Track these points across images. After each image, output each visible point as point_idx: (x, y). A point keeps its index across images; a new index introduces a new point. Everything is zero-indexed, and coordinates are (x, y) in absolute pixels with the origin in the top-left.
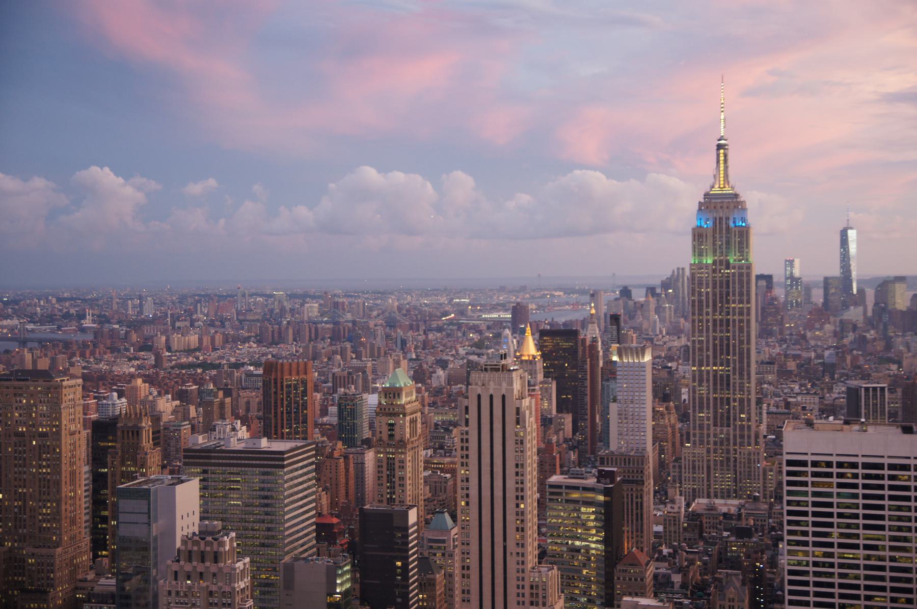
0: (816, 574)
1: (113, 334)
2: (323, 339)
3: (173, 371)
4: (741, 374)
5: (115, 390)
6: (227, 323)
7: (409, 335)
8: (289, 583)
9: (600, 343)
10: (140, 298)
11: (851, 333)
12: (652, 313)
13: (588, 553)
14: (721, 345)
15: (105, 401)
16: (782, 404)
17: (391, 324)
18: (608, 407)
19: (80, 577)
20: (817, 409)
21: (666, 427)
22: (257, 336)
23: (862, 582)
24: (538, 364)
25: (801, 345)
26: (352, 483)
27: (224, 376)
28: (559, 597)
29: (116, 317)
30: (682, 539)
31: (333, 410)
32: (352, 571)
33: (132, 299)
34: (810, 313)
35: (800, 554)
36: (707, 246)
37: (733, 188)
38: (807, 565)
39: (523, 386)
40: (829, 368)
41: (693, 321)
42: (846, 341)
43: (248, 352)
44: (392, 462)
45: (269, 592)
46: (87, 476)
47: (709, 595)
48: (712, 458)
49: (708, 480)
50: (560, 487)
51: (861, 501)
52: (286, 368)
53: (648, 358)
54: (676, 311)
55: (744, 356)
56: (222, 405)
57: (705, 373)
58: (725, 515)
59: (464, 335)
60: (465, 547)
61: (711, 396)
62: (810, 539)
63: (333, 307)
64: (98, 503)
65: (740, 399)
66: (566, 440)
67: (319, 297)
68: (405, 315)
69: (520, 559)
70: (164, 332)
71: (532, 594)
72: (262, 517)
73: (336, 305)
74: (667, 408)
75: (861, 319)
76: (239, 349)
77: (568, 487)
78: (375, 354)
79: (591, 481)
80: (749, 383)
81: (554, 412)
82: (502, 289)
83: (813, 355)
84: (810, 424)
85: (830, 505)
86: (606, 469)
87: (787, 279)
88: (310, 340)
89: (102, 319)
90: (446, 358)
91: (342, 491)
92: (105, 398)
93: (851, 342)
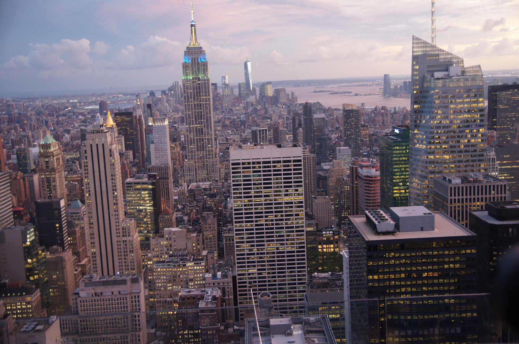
0: (245, 209)
4: (208, 128)
12: (165, 103)
14: (198, 115)
17: (39, 113)
21: (175, 153)
23: (264, 211)
26: (28, 190)
28: (136, 232)
31: (14, 156)
32: (35, 231)
34: (234, 99)
35: (239, 202)
36: (189, 71)
38: (242, 206)
39: (112, 139)
40: (243, 123)
41: (185, 105)
42: (249, 111)
47: (200, 223)
48: (197, 165)
49: (196, 175)
50: (131, 183)
51: (262, 178)
53: (166, 123)
55: (208, 119)
58: (204, 189)
60: (90, 215)
61: (195, 138)
66: (131, 163)
68: (46, 109)
71: (123, 232)
73: (9, 106)
74: (175, 145)
75: (255, 101)
77: (135, 183)
79: (146, 180)
81: (124, 150)
82: (93, 95)
84: (240, 147)
90: (69, 128)
91: (23, 195)
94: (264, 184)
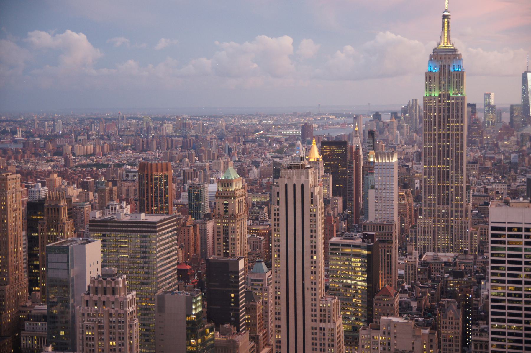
0: (509, 301)
1: (35, 143)
2: (176, 148)
3: (77, 169)
4: (457, 170)
5: (39, 182)
6: (112, 137)
7: (233, 145)
8: (161, 308)
9: (361, 150)
10: (53, 120)
11: (528, 143)
13: (356, 288)
14: (444, 151)
15: (33, 189)
16: (483, 190)
17: (221, 137)
18: (368, 193)
19: (22, 304)
20: (505, 193)
21: (405, 205)
22: (132, 146)
24: (320, 164)
25: (495, 151)
26: (198, 242)
27: (111, 172)
28: (339, 317)
29: (37, 133)
30: (417, 279)
31: (185, 194)
32: (203, 300)
33: (47, 121)
34: (501, 129)
35: (500, 288)
37: (453, 45)
38: (504, 296)
39: (315, 179)
40: (514, 166)
41: (425, 135)
43: (127, 157)
44: (226, 228)
45: (148, 314)
46: (24, 238)
49: (434, 240)
50: (338, 245)
52: (154, 167)
53: (395, 159)
54: (411, 128)
55: (459, 158)
56: (111, 191)
57: (432, 169)
58: (445, 263)
59: (270, 145)
60: (277, 284)
61: (437, 185)
62: (506, 278)
63: (183, 126)
64: (32, 256)
65: (456, 186)
66: (339, 214)
67: (173, 120)
68: (230, 132)
69: (314, 292)
70: (70, 143)
71: (321, 315)
72: (142, 265)
73: (184, 125)
74: (406, 193)
76: (120, 154)
77: (343, 245)
78: (212, 158)
79: (359, 241)
80: (462, 176)
81: (331, 196)
82: (294, 114)
83: (502, 157)
84: (507, 203)
85: (520, 256)
86: (368, 233)
87: (485, 106)
88: (168, 148)
89: (28, 134)
90: (258, 160)
91: (192, 248)
92: (32, 187)
93: (528, 149)
94: (520, 263)
